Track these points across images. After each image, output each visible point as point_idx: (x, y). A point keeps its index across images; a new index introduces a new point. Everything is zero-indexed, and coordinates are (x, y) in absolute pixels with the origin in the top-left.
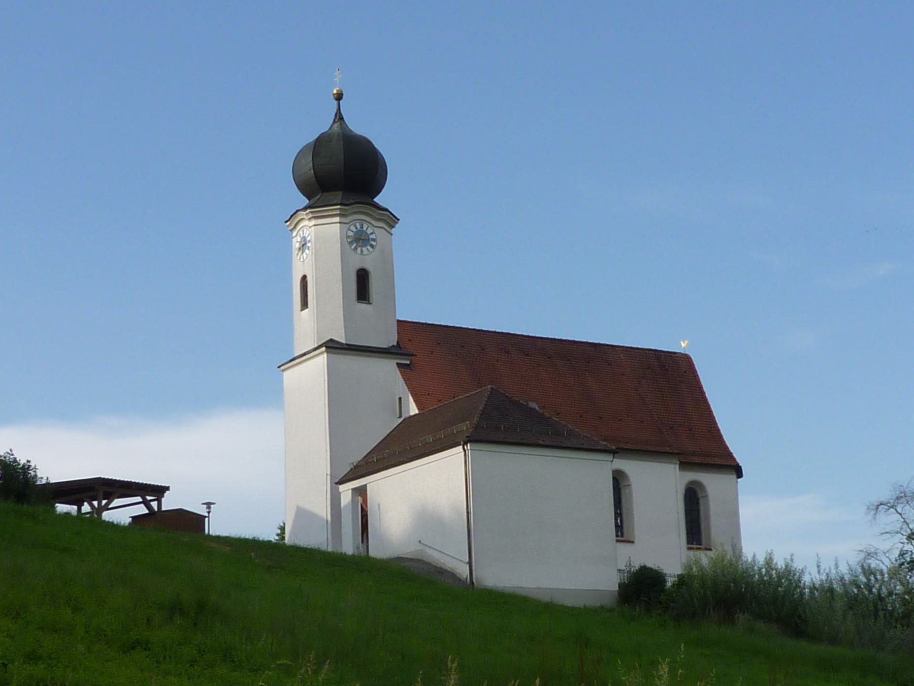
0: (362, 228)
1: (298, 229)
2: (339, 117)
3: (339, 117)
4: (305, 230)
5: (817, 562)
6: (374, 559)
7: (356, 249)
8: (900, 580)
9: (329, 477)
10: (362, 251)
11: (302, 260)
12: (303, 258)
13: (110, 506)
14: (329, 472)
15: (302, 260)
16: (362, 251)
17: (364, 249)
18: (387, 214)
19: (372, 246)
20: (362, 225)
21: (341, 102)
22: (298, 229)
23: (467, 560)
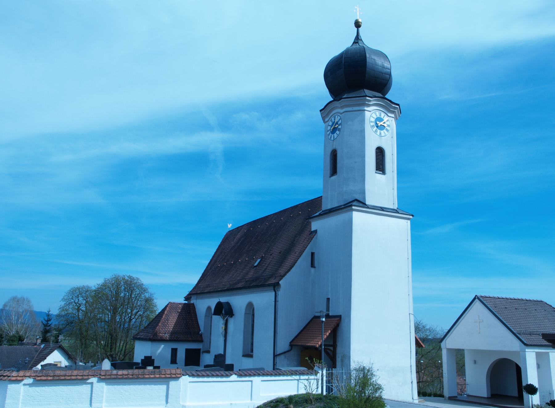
0: (381, 116)
1: (330, 116)
2: (358, 39)
3: (358, 39)
4: (336, 116)
5: (45, 325)
6: (165, 385)
7: (376, 131)
8: (128, 333)
9: (412, 316)
10: (380, 133)
11: (332, 139)
12: (334, 137)
13: (248, 371)
14: (412, 312)
15: (332, 139)
16: (380, 133)
17: (382, 132)
18: (343, 101)
19: (387, 130)
20: (381, 114)
21: (360, 29)
22: (330, 116)
23: (26, 375)
